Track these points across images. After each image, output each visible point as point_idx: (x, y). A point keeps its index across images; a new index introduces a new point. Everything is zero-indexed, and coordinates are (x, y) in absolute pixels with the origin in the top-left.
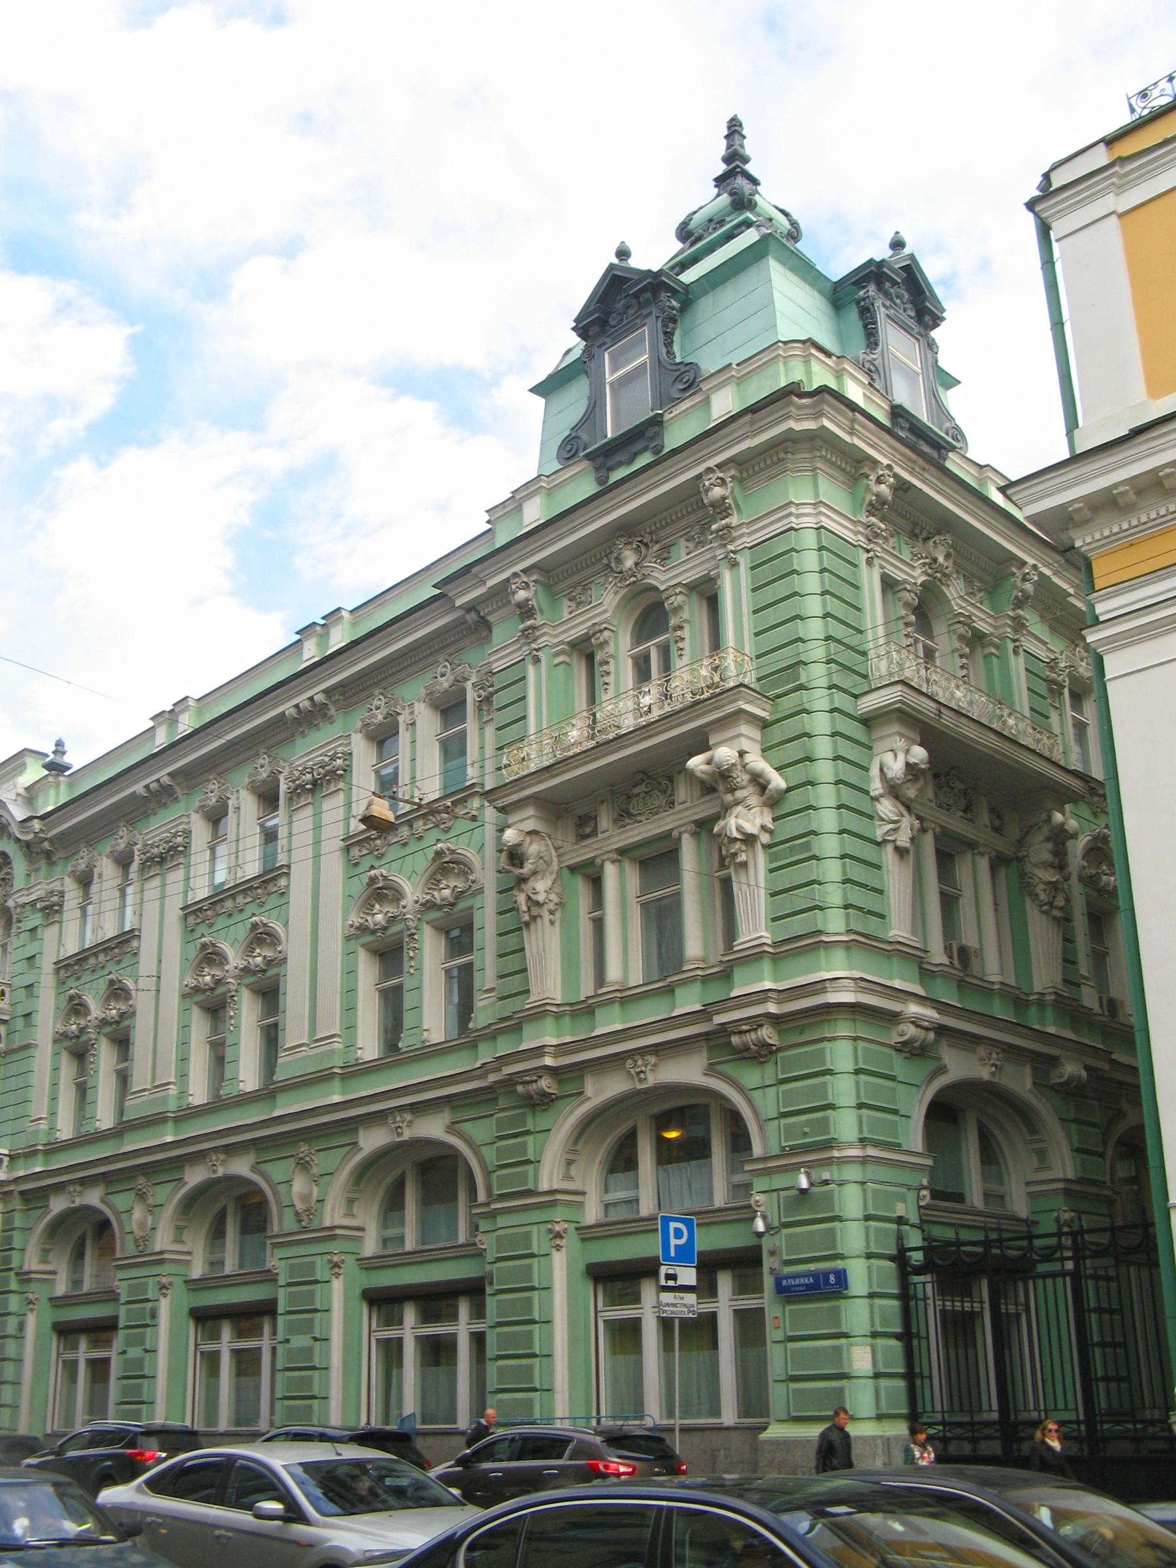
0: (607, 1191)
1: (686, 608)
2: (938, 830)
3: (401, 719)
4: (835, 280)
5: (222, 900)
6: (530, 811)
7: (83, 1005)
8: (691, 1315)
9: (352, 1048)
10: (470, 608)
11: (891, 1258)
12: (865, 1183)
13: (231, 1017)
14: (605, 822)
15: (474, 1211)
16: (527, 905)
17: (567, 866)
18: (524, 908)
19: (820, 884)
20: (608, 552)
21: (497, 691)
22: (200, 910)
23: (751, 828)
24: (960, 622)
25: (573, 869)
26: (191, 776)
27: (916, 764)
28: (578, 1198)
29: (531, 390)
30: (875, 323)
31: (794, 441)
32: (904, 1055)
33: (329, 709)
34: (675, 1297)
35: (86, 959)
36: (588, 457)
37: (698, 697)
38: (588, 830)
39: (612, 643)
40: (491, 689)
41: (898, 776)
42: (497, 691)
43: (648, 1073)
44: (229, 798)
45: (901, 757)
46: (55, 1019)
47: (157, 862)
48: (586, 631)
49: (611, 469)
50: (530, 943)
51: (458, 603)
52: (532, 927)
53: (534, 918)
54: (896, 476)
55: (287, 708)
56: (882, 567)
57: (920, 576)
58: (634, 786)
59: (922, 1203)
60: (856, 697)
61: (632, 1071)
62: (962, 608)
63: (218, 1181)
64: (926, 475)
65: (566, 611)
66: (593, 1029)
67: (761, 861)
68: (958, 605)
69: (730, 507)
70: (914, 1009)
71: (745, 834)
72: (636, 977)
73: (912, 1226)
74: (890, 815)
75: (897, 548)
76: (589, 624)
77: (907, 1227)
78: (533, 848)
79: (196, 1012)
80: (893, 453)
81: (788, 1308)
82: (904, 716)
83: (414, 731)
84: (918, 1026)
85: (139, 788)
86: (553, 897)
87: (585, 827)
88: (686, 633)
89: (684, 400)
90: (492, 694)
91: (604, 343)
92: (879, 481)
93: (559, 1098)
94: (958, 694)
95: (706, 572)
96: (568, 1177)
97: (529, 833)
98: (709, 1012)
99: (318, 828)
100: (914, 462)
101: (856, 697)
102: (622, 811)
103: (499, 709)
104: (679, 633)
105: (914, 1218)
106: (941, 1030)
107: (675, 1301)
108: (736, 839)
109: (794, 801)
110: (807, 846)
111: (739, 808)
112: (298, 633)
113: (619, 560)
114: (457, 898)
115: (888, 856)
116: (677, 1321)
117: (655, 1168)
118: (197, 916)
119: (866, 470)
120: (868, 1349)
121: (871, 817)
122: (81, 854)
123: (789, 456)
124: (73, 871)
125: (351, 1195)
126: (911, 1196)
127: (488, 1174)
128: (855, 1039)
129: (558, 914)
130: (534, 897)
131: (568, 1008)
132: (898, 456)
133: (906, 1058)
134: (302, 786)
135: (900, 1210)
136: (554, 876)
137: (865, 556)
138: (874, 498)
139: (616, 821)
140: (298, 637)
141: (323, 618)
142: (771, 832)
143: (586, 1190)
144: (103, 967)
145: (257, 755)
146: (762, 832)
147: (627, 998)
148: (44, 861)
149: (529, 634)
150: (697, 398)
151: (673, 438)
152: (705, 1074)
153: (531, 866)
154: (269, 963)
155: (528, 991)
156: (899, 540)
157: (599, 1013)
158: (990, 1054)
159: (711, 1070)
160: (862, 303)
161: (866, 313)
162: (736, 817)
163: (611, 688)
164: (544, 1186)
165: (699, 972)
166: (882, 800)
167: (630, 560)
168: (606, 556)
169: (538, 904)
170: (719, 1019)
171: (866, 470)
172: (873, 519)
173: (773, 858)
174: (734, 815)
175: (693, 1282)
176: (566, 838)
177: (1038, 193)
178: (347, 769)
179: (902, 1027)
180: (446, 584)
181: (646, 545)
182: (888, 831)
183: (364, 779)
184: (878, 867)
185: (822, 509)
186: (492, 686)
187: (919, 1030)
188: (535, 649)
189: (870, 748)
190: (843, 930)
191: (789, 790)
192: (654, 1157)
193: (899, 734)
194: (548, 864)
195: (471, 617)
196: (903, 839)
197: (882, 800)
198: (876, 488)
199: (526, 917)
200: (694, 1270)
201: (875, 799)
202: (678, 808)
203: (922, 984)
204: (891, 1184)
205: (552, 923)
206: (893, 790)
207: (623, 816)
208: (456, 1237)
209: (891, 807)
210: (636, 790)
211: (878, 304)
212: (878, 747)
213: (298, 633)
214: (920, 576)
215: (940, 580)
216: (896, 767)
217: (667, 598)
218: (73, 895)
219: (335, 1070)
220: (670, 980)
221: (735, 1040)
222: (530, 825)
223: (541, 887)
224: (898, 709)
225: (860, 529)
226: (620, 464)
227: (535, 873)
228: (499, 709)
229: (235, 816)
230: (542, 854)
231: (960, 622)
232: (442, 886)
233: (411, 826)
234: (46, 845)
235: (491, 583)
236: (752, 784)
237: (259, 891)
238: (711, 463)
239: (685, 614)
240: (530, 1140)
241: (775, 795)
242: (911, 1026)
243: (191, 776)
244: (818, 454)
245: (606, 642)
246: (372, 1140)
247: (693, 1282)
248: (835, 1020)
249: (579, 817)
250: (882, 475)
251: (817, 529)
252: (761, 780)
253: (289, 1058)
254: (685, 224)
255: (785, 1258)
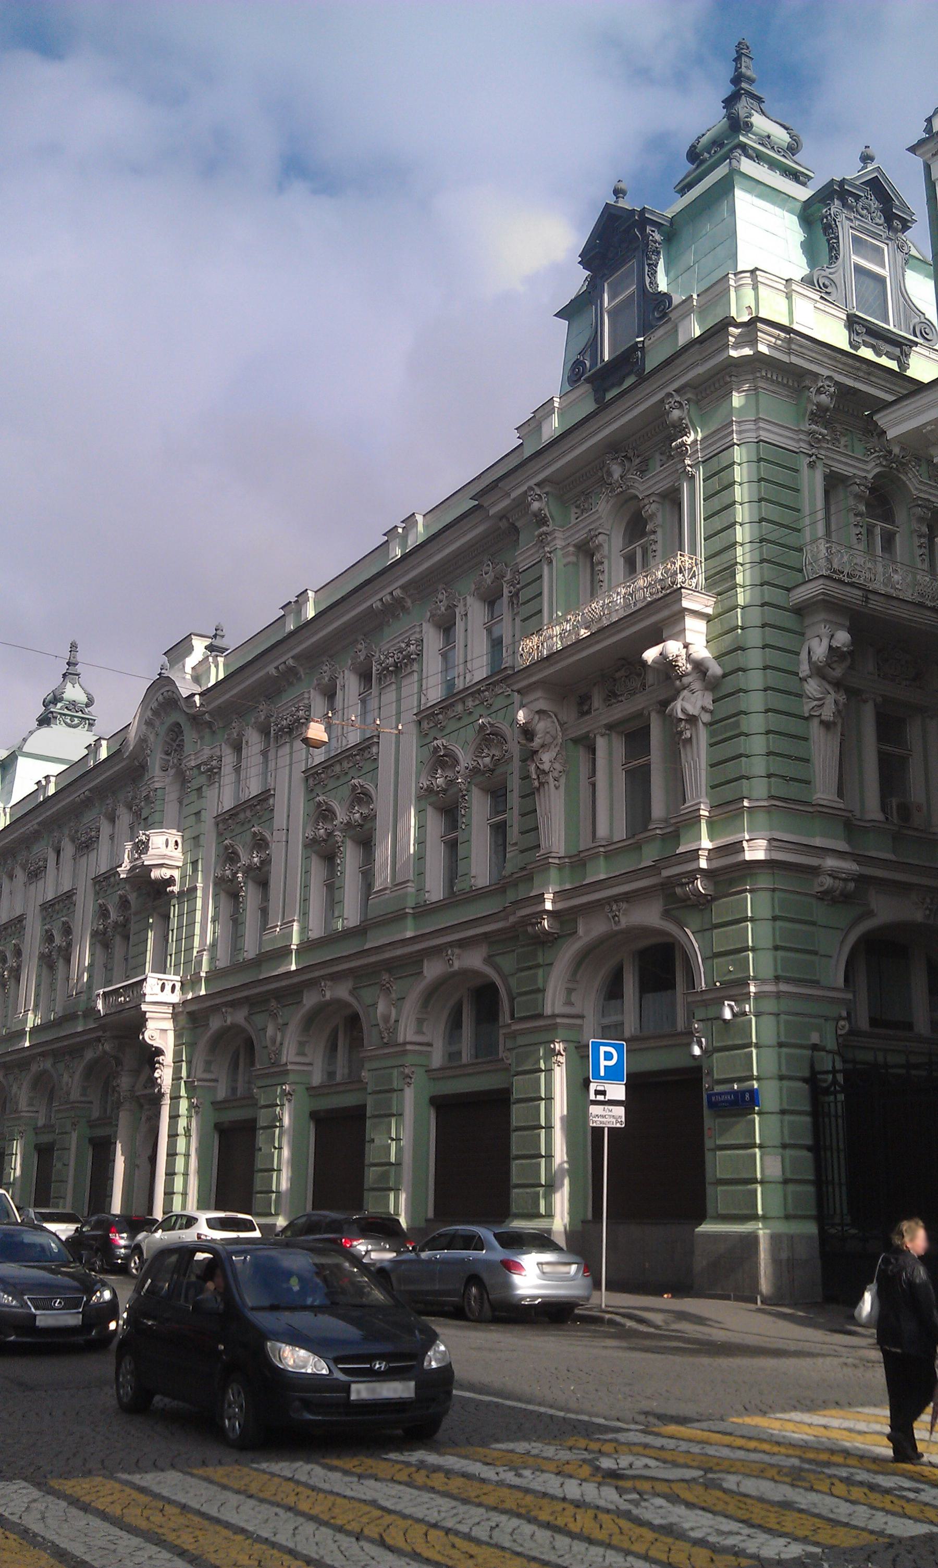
0: (603, 1016)
1: (659, 515)
2: (879, 699)
3: (457, 611)
4: (804, 200)
5: (331, 765)
6: (539, 694)
7: (235, 853)
8: (618, 1125)
9: (422, 891)
10: (502, 516)
11: (805, 1080)
12: (779, 1014)
13: (338, 865)
14: (597, 702)
15: (690, 999)
16: (536, 773)
17: (571, 739)
18: (534, 776)
19: (748, 757)
20: (602, 465)
21: (522, 588)
22: (316, 773)
23: (692, 710)
24: (919, 506)
25: (576, 741)
26: (312, 658)
27: (838, 648)
28: (578, 1021)
29: (555, 315)
30: (837, 238)
31: (736, 366)
32: (826, 903)
33: (406, 602)
34: (604, 1110)
35: (236, 814)
36: (588, 380)
37: (655, 597)
38: (586, 708)
39: (606, 546)
40: (518, 586)
41: (820, 659)
42: (522, 588)
43: (621, 916)
44: (337, 678)
45: (825, 642)
46: (216, 864)
47: (287, 732)
48: (586, 535)
49: (606, 390)
50: (540, 805)
51: (491, 512)
52: (541, 791)
53: (542, 784)
54: (837, 383)
55: (374, 602)
56: (826, 465)
57: (873, 468)
58: (617, 671)
59: (840, 1032)
60: (788, 590)
61: (610, 915)
62: (921, 491)
63: (455, 974)
64: (873, 379)
65: (573, 516)
66: (584, 879)
67: (703, 736)
68: (917, 489)
69: (687, 427)
70: (830, 863)
71: (688, 715)
72: (621, 833)
73: (829, 1052)
74: (815, 693)
75: (850, 448)
76: (587, 530)
77: (823, 1053)
78: (541, 726)
79: (314, 858)
80: (835, 364)
81: (717, 1121)
82: (828, 604)
83: (467, 619)
84: (835, 878)
85: (271, 670)
86: (557, 766)
87: (583, 705)
88: (659, 536)
89: (660, 327)
90: (519, 590)
91: (604, 275)
92: (819, 392)
93: (560, 937)
94: (896, 577)
95: (672, 483)
96: (569, 1003)
97: (539, 712)
98: (659, 867)
99: (399, 700)
100: (858, 369)
101: (788, 590)
102: (610, 692)
103: (524, 603)
104: (652, 537)
105: (831, 1044)
106: (861, 880)
107: (604, 1113)
108: (681, 720)
109: (729, 685)
110: (737, 725)
111: (685, 693)
112: (385, 535)
113: (610, 474)
114: (495, 766)
115: (815, 729)
116: (606, 1130)
117: (637, 994)
118: (315, 778)
119: (807, 383)
120: (779, 1158)
121: (800, 696)
122: (234, 724)
123: (734, 379)
124: (228, 739)
125: (570, 986)
126: (829, 1027)
127: (512, 1000)
128: (774, 890)
129: (563, 780)
130: (541, 767)
131: (567, 860)
132: (840, 366)
133: (828, 905)
134: (386, 668)
135: (815, 1038)
136: (558, 748)
137: (808, 460)
138: (815, 407)
139: (605, 700)
140: (386, 538)
141: (402, 522)
142: (711, 712)
143: (585, 1013)
144: (249, 821)
145: (356, 641)
146: (703, 712)
147: (612, 852)
148: (207, 730)
149: (542, 541)
150: (669, 326)
151: (651, 363)
152: (663, 919)
153: (539, 740)
154: (364, 818)
155: (539, 846)
156: (852, 439)
157: (589, 866)
158: (924, 899)
159: (666, 914)
160: (825, 220)
161: (829, 229)
162: (682, 700)
163: (605, 584)
164: (548, 1011)
165: (658, 831)
166: (809, 680)
167: (617, 471)
168: (601, 469)
169: (544, 772)
170: (666, 873)
171: (807, 383)
172: (814, 427)
173: (712, 734)
174: (681, 697)
175: (622, 1097)
176: (569, 714)
177: (924, 135)
178: (420, 655)
179: (821, 879)
180: (482, 496)
181: (630, 460)
182: (813, 708)
183: (432, 663)
184: (806, 739)
185: (761, 425)
186: (518, 583)
187: (837, 881)
188: (548, 552)
189: (803, 634)
190: (765, 796)
191: (725, 676)
192: (637, 985)
193: (825, 621)
194: (555, 738)
195: (504, 524)
196: (828, 713)
197: (809, 680)
198: (815, 399)
199: (536, 783)
200: (624, 1086)
201: (803, 680)
202: (648, 689)
203: (849, 842)
204: (810, 1016)
205: (557, 788)
206: (818, 671)
207: (611, 697)
208: (674, 1023)
209: (816, 687)
210: (618, 675)
211: (841, 218)
212: (809, 633)
213: (385, 535)
214: (873, 468)
215: (897, 470)
216: (820, 650)
217: (644, 507)
218: (229, 759)
219: (407, 910)
220: (637, 837)
221: (678, 890)
222: (542, 705)
223: (546, 757)
224: (823, 600)
225: (801, 436)
226: (613, 386)
227: (543, 746)
228: (524, 603)
229: (341, 693)
230: (548, 730)
231: (919, 506)
232: (484, 754)
233: (464, 703)
234: (207, 716)
235: (513, 495)
236: (696, 671)
237: (358, 757)
238: (670, 389)
239: (659, 519)
240: (540, 972)
241: (713, 681)
242: (828, 878)
243: (312, 658)
244: (758, 375)
245: (600, 545)
246: (432, 970)
247: (622, 1097)
248: (756, 874)
249: (580, 697)
250: (822, 387)
251: (757, 442)
252: (703, 668)
253: (376, 900)
254: (693, 147)
255: (716, 1077)
